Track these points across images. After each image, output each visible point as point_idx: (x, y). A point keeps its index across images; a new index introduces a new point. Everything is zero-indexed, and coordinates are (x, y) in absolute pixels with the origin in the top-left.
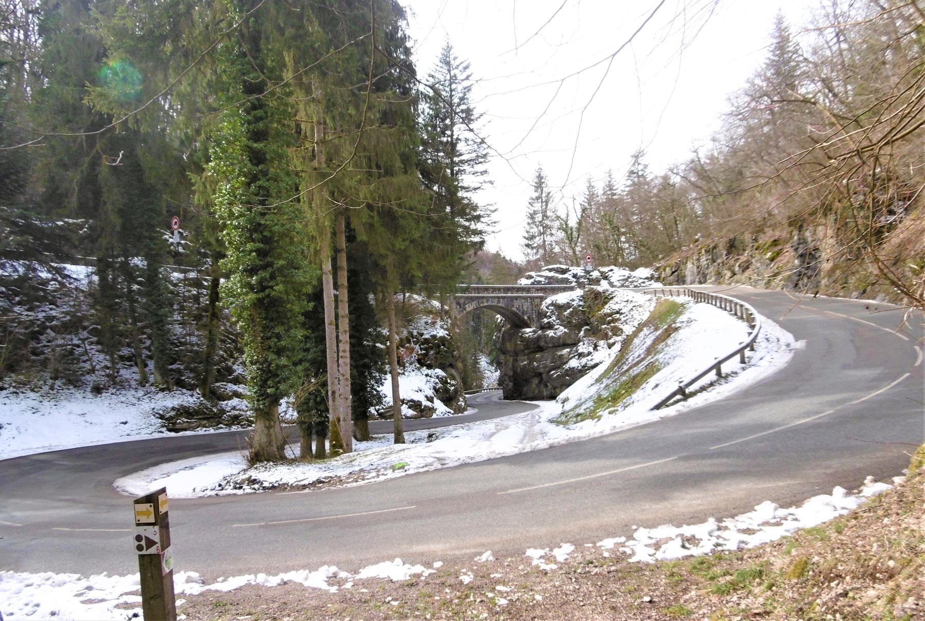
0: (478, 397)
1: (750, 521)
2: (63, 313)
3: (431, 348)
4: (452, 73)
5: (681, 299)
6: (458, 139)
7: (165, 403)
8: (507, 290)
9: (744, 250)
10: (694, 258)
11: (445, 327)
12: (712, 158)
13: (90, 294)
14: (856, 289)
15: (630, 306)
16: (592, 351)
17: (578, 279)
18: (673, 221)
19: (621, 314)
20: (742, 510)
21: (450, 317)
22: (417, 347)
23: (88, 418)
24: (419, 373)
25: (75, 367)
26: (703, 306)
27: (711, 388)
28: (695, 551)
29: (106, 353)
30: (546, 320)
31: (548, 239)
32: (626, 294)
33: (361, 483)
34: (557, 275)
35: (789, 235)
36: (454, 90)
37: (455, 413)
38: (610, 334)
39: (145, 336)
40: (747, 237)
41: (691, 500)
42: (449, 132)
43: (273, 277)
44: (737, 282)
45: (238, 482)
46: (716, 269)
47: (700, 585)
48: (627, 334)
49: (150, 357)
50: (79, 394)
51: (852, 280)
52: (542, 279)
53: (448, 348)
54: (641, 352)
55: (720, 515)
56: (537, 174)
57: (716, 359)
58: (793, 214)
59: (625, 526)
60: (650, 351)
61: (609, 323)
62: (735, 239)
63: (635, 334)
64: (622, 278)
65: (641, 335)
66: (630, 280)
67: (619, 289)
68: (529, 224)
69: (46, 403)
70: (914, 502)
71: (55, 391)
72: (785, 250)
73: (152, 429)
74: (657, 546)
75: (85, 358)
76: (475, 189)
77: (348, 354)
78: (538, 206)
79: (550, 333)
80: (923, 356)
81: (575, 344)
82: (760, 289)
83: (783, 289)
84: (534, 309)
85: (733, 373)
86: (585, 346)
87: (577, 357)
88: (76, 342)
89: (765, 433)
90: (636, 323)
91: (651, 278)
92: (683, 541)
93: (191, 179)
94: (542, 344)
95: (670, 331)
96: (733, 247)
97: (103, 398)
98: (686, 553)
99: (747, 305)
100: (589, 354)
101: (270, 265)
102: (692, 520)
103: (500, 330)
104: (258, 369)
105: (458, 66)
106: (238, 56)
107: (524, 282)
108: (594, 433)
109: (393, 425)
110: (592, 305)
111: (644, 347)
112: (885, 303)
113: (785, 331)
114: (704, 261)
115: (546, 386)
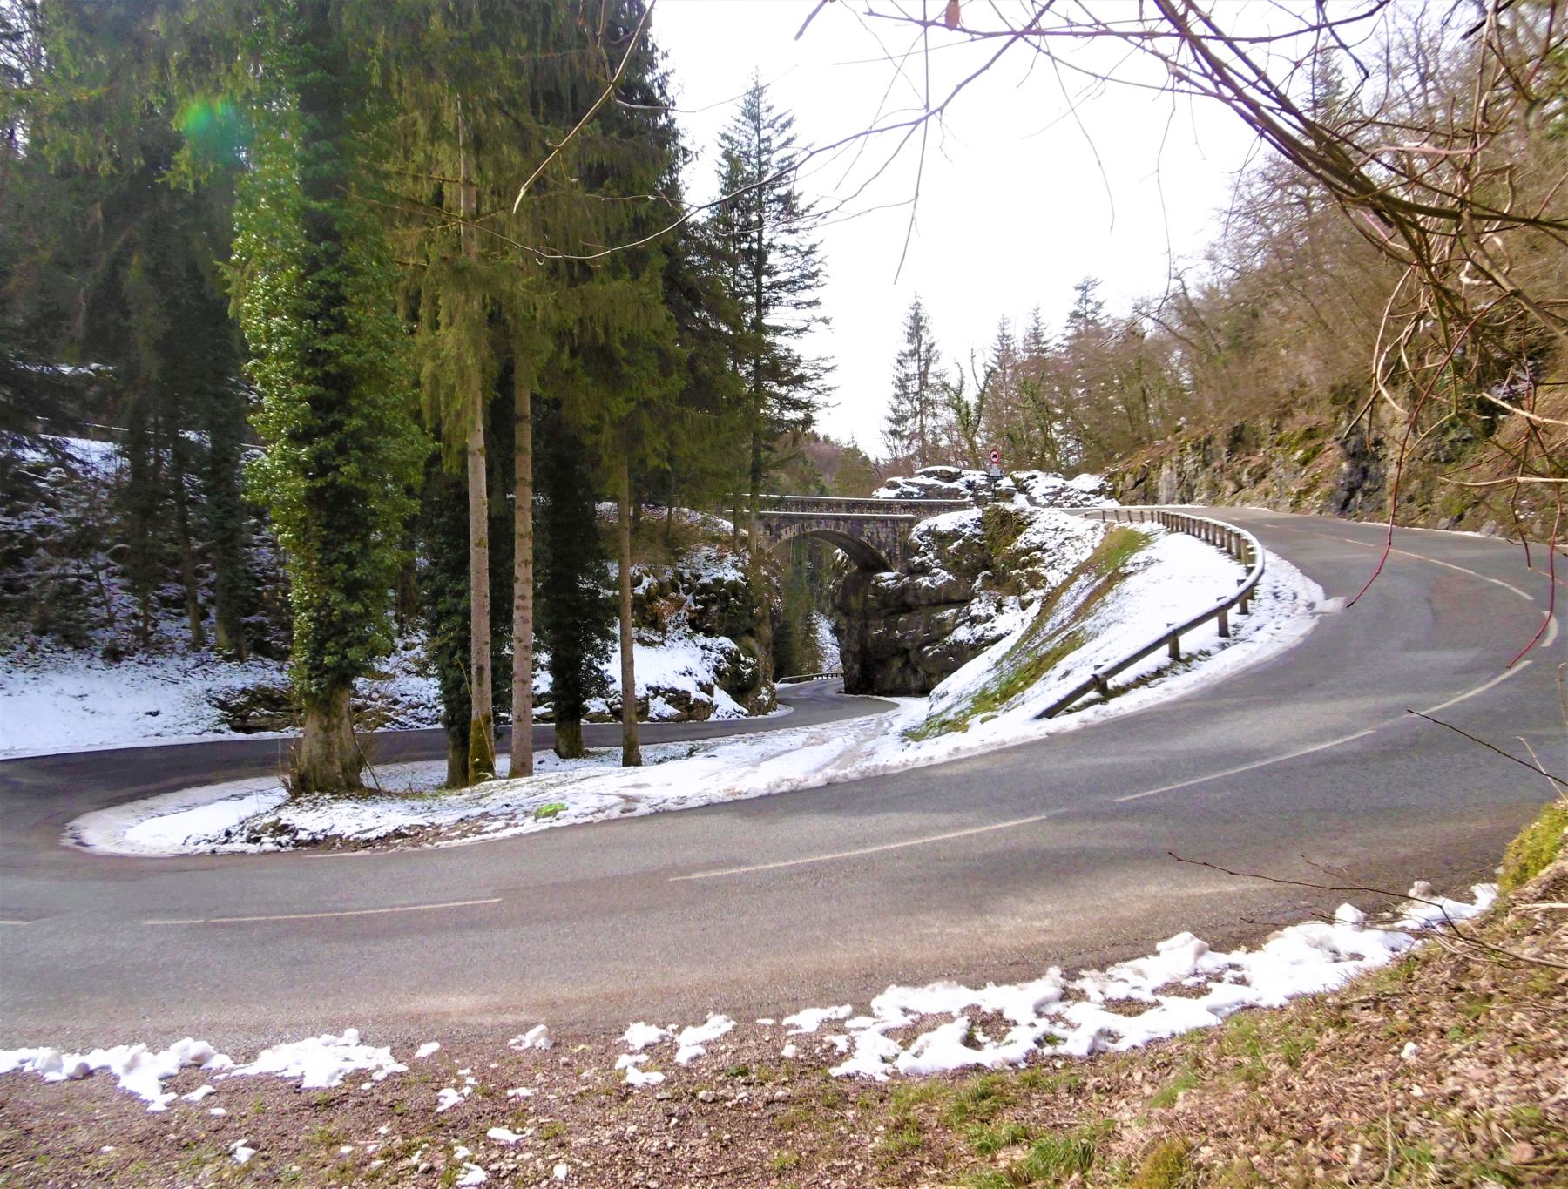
0: (802, 688)
1: (1139, 981)
2: (66, 520)
3: (714, 601)
4: (764, 134)
5: (1146, 527)
6: (770, 246)
7: (229, 682)
8: (852, 506)
9: (1258, 447)
10: (1174, 459)
11: (740, 565)
12: (1211, 293)
13: (117, 490)
14: (1447, 512)
15: (1060, 537)
16: (993, 613)
17: (976, 490)
18: (1140, 394)
19: (1045, 551)
20: (1127, 951)
21: (749, 549)
22: (690, 597)
23: (89, 703)
24: (691, 643)
25: (79, 614)
26: (1182, 540)
27: (1157, 680)
28: (991, 1055)
29: (134, 592)
30: (917, 559)
31: (930, 422)
32: (1054, 517)
33: (472, 838)
34: (939, 483)
35: (1332, 420)
36: (765, 163)
37: (751, 713)
38: (1026, 584)
39: (208, 565)
40: (1264, 423)
41: (1031, 918)
42: (755, 234)
43: (341, 449)
44: (1244, 501)
45: (257, 828)
46: (1210, 477)
47: (950, 1167)
48: (1054, 584)
49: (211, 601)
50: (79, 662)
51: (1440, 496)
52: (915, 490)
53: (743, 602)
54: (1067, 615)
55: (1074, 960)
56: (913, 313)
57: (1169, 625)
58: (1339, 383)
59: (867, 976)
60: (1081, 613)
61: (1024, 565)
62: (1242, 427)
63: (1065, 586)
64: (1051, 490)
65: (1074, 587)
66: (1064, 494)
67: (1046, 510)
68: (897, 396)
69: (18, 675)
70: (1489, 998)
71: (37, 655)
72: (1327, 447)
73: (204, 725)
74: (907, 1036)
75: (98, 599)
76: (798, 331)
77: (530, 603)
78: (912, 367)
79: (925, 581)
80: (1560, 630)
81: (965, 601)
82: (1284, 512)
83: (1321, 512)
84: (898, 539)
85: (1201, 652)
86: (983, 605)
87: (968, 623)
88: (85, 571)
89: (1231, 772)
90: (1069, 568)
91: (1099, 492)
92: (973, 1024)
93: (223, 274)
94: (910, 599)
95: (1119, 577)
96: (1238, 440)
97: (122, 669)
98: (970, 1057)
99: (1247, 535)
100: (989, 618)
101: (337, 426)
102: (1013, 970)
103: (841, 574)
104: (311, 619)
105: (774, 122)
106: (291, 42)
107: (883, 494)
108: (916, 760)
109: (621, 732)
110: (995, 535)
111: (1072, 607)
112: (1496, 538)
113: (1309, 581)
114: (1189, 464)
115: (915, 672)
